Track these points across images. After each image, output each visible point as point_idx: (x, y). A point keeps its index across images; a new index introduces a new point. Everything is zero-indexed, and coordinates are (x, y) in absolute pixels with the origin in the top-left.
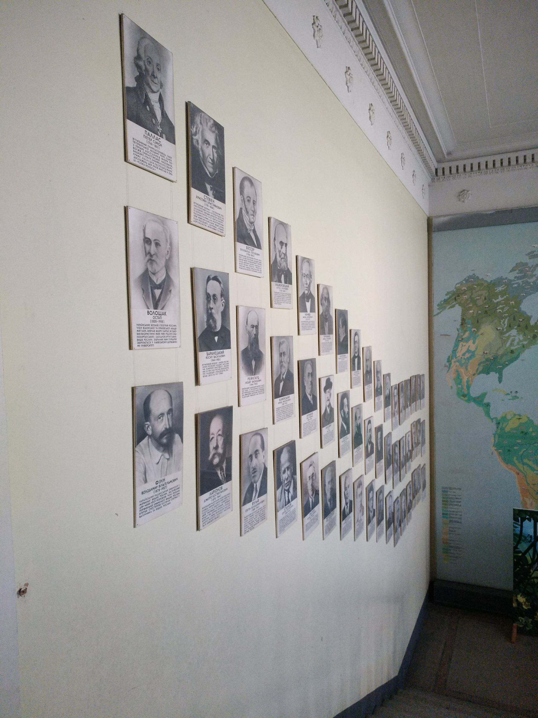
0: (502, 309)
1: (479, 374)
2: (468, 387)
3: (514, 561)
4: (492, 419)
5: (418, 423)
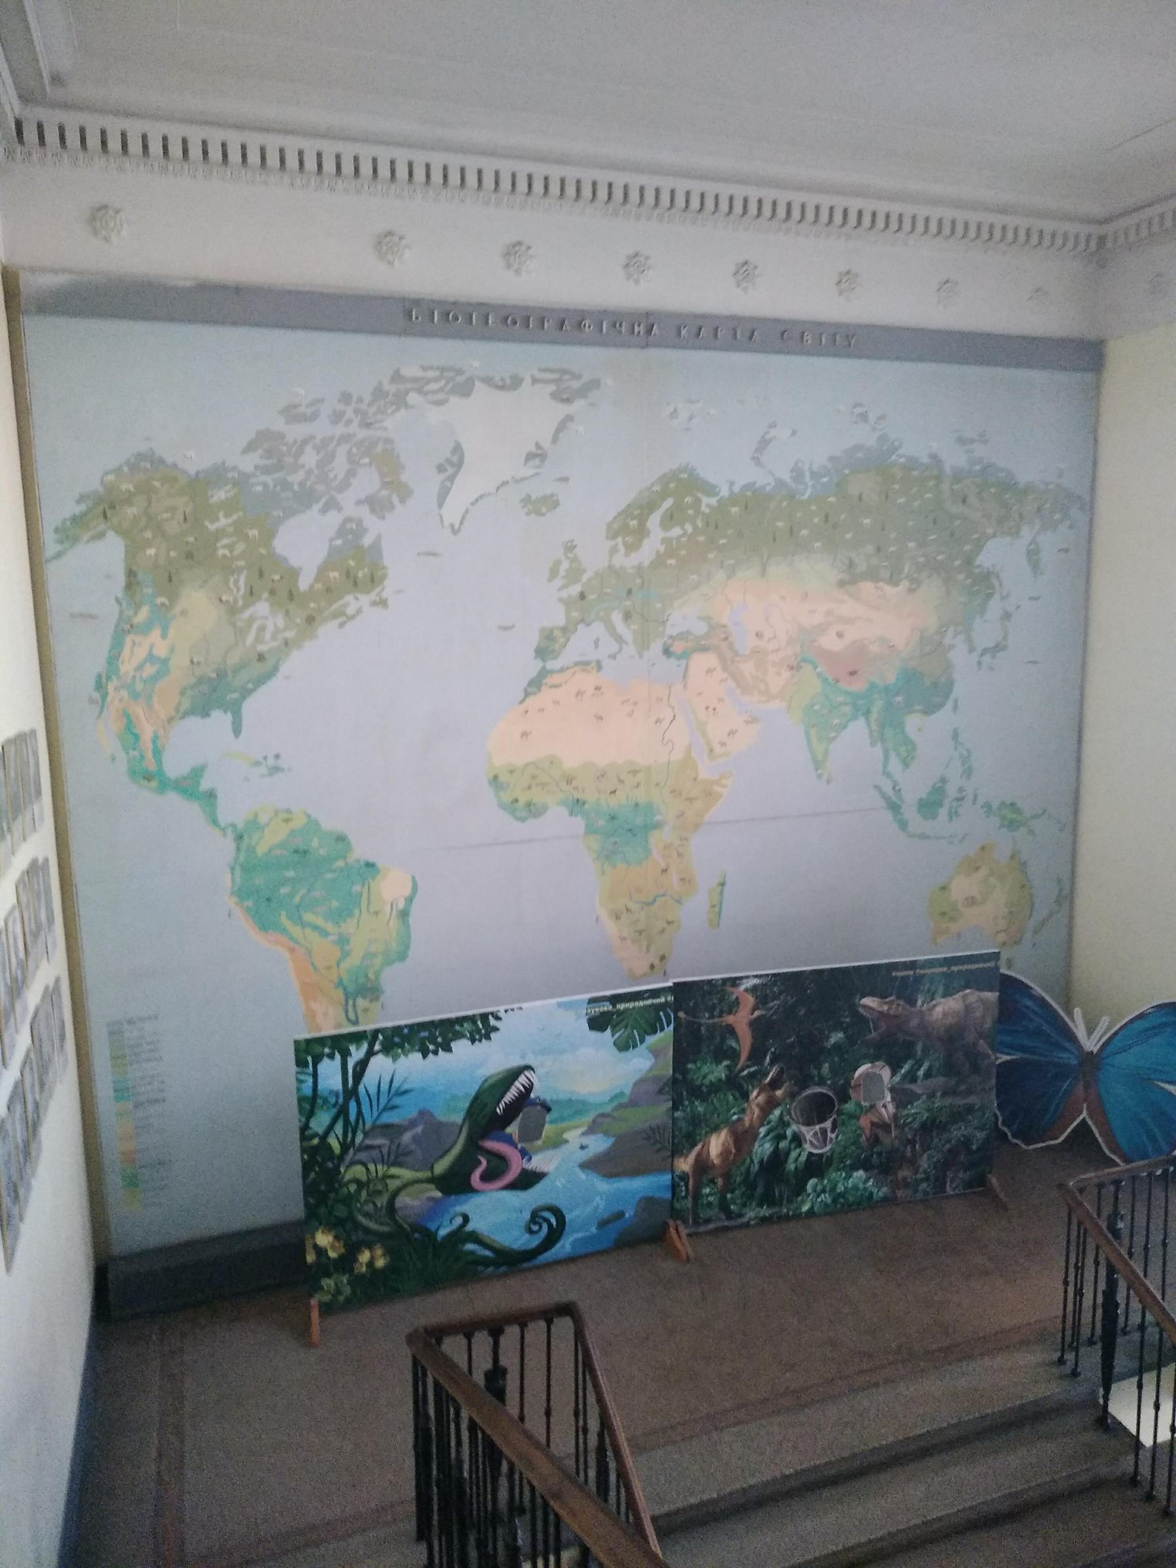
0: (230, 547)
1: (183, 717)
2: (158, 753)
3: (303, 1159)
4: (224, 830)
5: (35, 869)
